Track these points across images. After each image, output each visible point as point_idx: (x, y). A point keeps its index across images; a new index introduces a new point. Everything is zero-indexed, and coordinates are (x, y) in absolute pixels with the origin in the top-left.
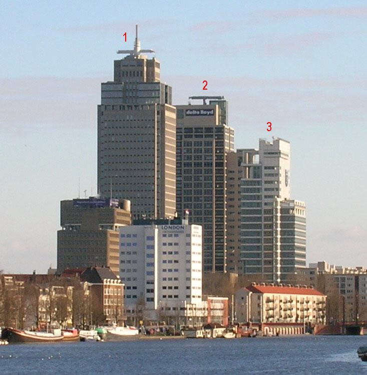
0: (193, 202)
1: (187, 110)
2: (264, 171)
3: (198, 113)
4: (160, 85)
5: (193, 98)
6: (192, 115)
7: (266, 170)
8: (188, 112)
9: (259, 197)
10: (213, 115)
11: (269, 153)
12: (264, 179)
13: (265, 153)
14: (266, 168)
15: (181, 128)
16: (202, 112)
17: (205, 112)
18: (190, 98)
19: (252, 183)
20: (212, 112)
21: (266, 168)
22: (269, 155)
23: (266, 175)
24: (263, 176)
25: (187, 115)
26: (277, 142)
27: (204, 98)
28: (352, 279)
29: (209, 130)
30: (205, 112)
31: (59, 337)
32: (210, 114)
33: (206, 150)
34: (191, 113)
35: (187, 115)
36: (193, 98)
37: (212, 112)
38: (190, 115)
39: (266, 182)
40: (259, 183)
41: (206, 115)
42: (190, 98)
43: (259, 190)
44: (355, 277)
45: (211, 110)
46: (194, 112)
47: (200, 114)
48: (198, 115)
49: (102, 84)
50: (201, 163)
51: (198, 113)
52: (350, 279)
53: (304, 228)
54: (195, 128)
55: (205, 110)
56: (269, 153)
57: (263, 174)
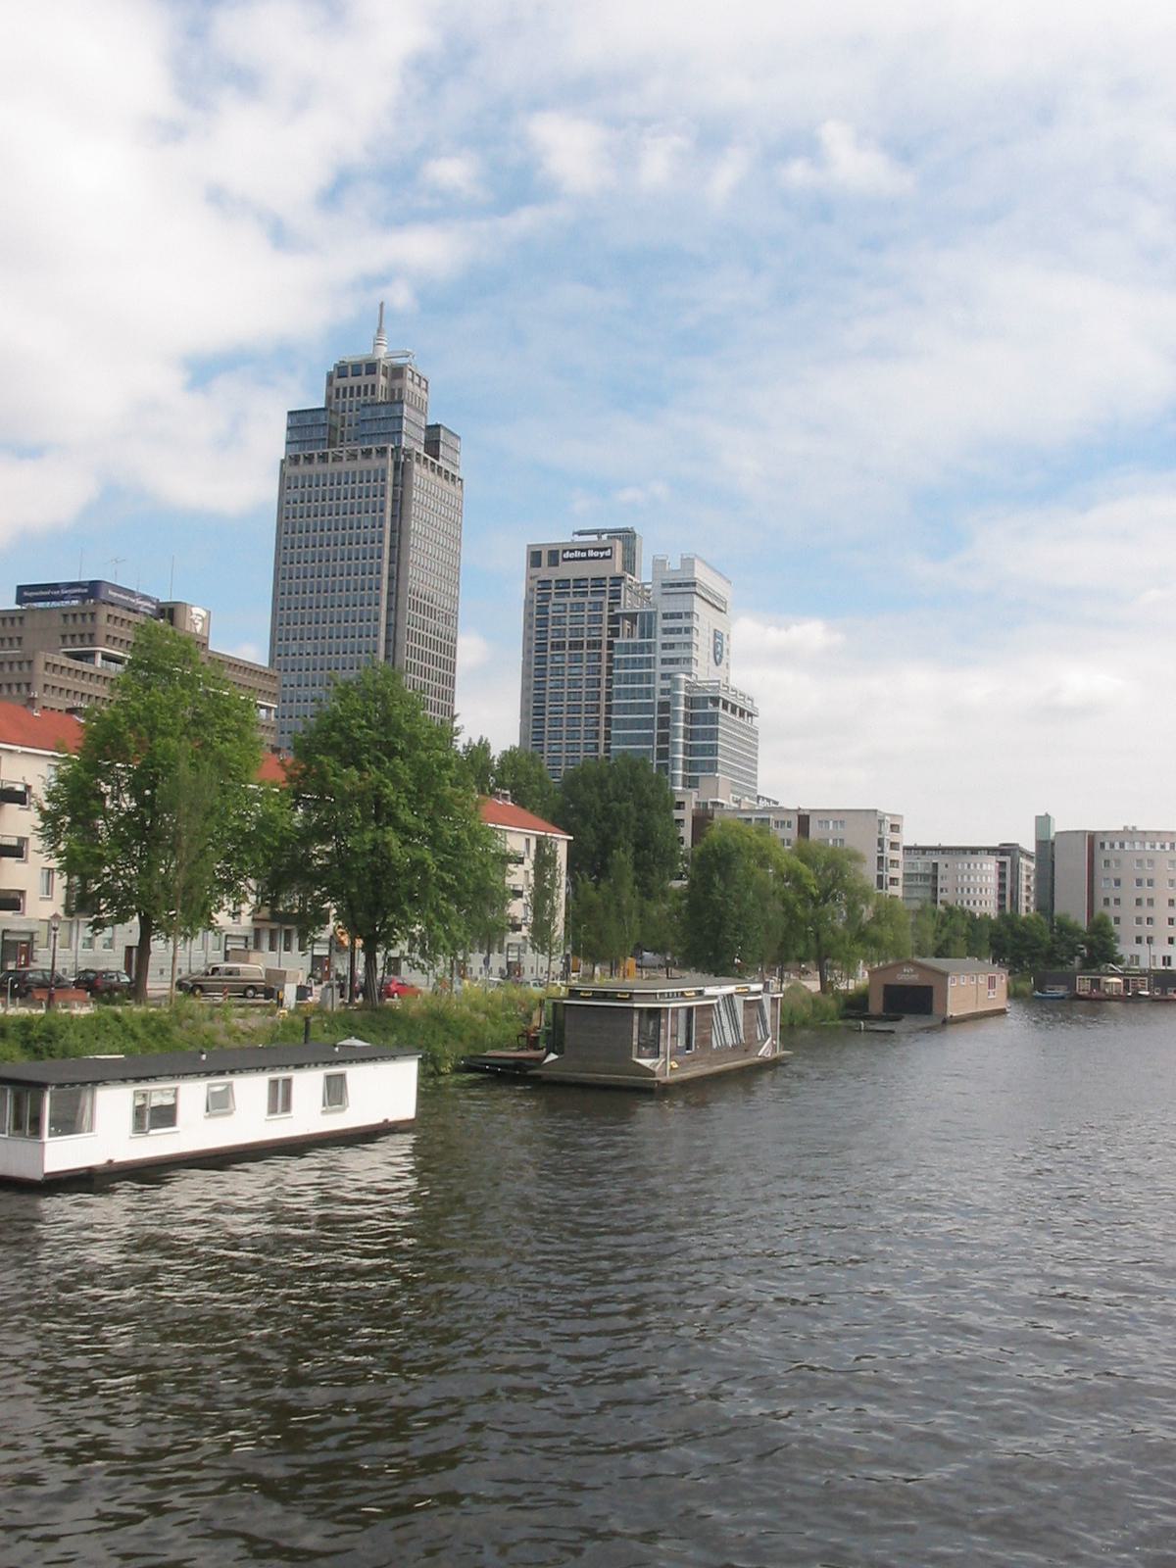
0: (583, 703)
1: (565, 551)
2: (661, 624)
3: (584, 555)
4: (442, 431)
5: (580, 533)
6: (575, 559)
7: (666, 621)
8: (567, 555)
9: (649, 678)
10: (609, 557)
11: (672, 585)
12: (660, 638)
13: (664, 585)
14: (665, 616)
15: (550, 581)
16: (591, 553)
17: (596, 554)
18: (575, 533)
19: (636, 648)
20: (608, 553)
21: (665, 616)
22: (672, 590)
23: (666, 631)
24: (659, 634)
25: (564, 560)
26: (688, 562)
27: (598, 533)
28: (789, 826)
29: (599, 581)
30: (596, 554)
31: (511, 831)
32: (605, 557)
33: (646, 650)
34: (571, 555)
35: (564, 560)
36: (580, 533)
37: (608, 553)
38: (569, 559)
39: (664, 646)
40: (649, 647)
41: (598, 558)
42: (575, 533)
43: (649, 662)
44: (800, 817)
45: (606, 549)
46: (577, 554)
47: (588, 558)
48: (583, 559)
49: (291, 413)
50: (588, 648)
51: (584, 555)
52: (783, 823)
53: (753, 780)
54: (575, 580)
55: (595, 550)
56: (672, 585)
57: (659, 628)
